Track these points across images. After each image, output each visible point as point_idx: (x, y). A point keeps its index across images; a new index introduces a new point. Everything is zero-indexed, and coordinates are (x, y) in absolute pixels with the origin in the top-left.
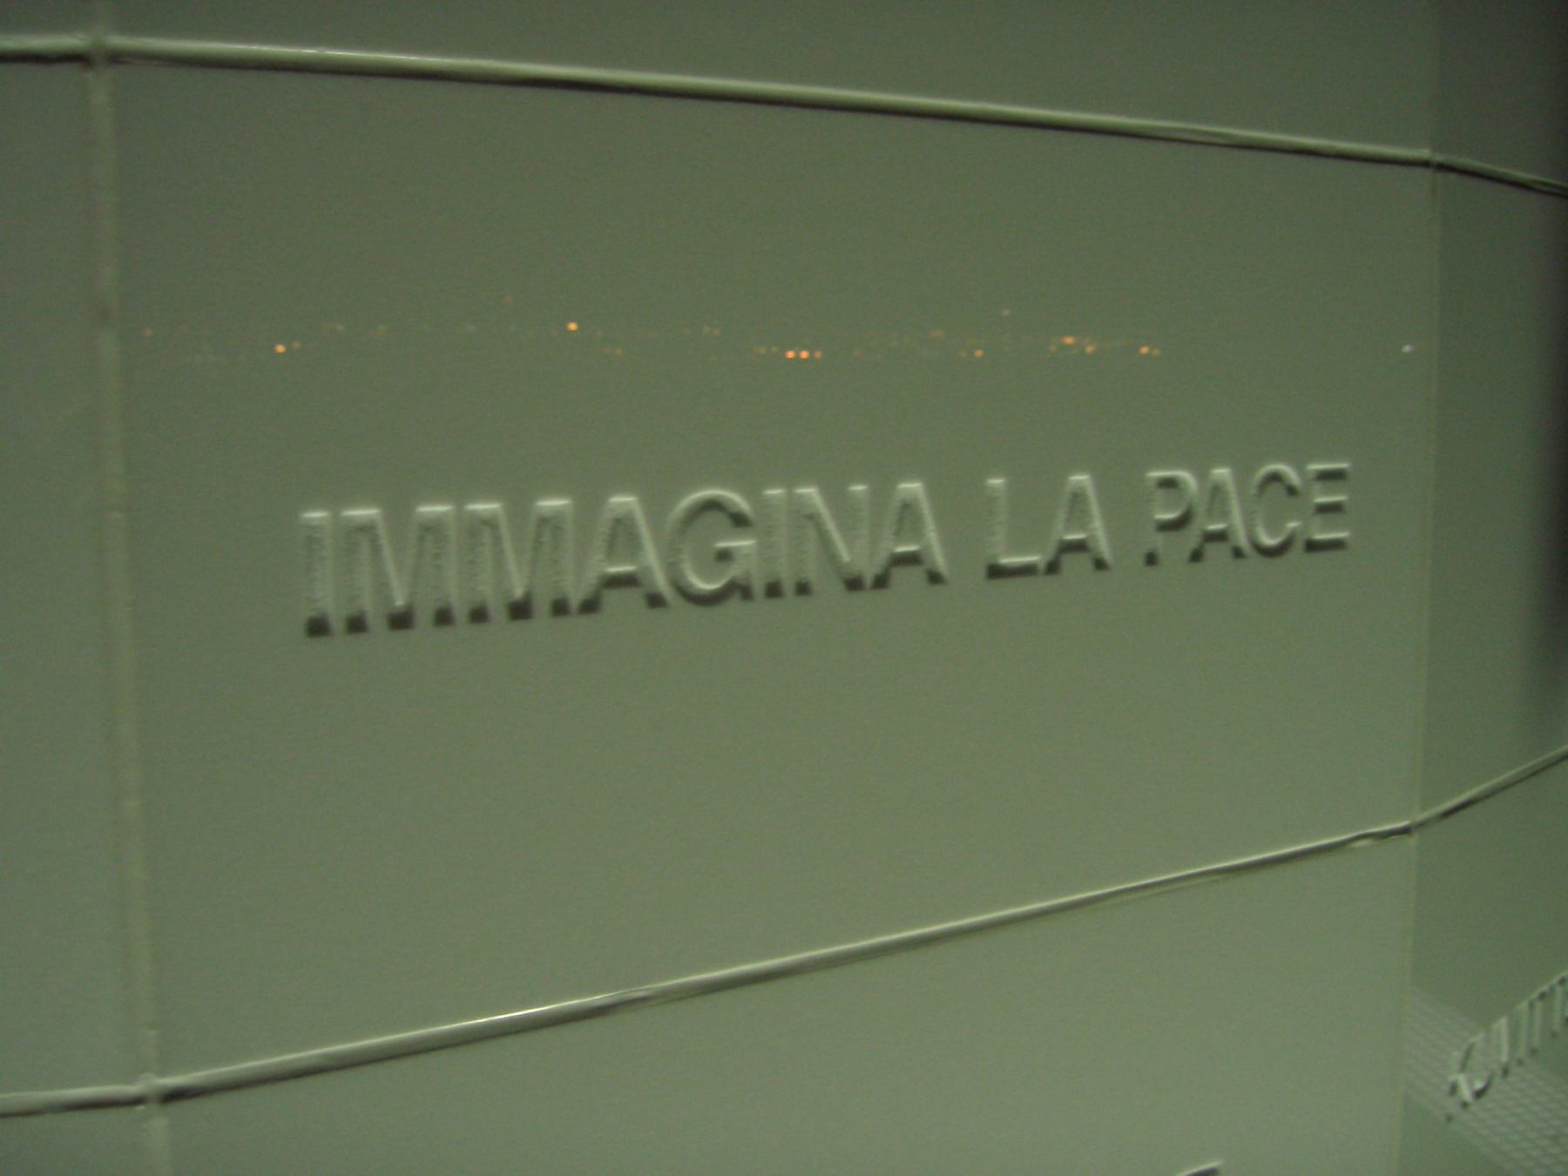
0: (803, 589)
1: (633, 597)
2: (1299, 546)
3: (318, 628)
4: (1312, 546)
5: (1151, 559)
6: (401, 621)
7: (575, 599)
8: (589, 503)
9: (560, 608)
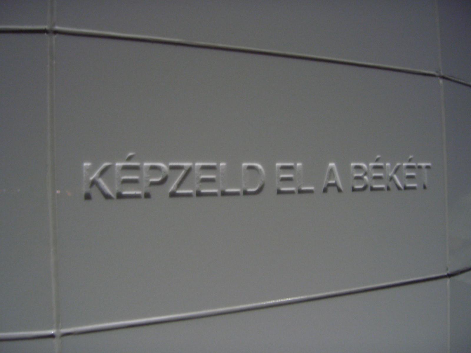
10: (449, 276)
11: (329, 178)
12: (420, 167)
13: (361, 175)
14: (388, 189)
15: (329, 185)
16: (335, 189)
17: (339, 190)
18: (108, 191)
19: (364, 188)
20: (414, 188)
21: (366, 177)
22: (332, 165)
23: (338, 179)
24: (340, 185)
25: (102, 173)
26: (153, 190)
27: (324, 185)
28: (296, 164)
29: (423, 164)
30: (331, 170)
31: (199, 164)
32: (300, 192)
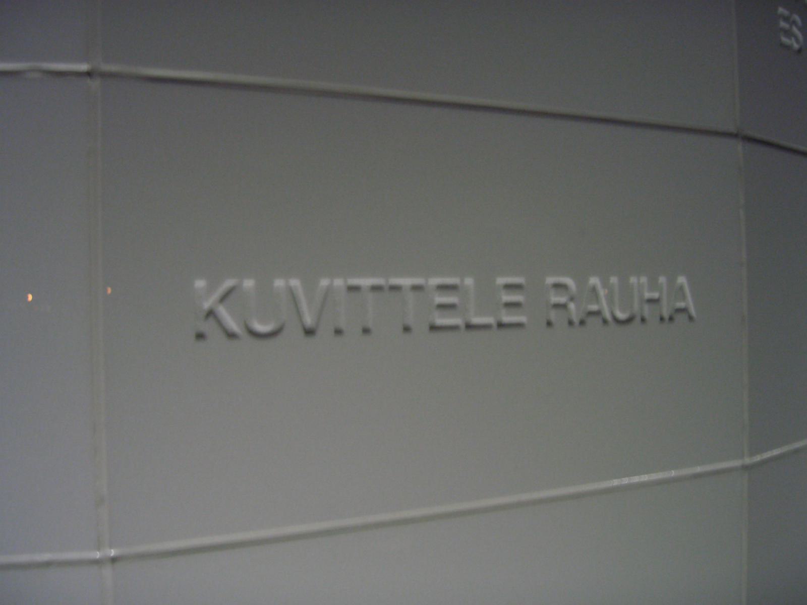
2: (638, 319)
12: (395, 288)
13: (562, 300)
15: (591, 313)
17: (691, 318)
18: (233, 325)
19: (630, 320)
20: (519, 325)
21: (572, 306)
23: (689, 303)
24: (693, 311)
25: (223, 299)
28: (462, 281)
29: (406, 282)
31: (435, 281)
32: (469, 326)
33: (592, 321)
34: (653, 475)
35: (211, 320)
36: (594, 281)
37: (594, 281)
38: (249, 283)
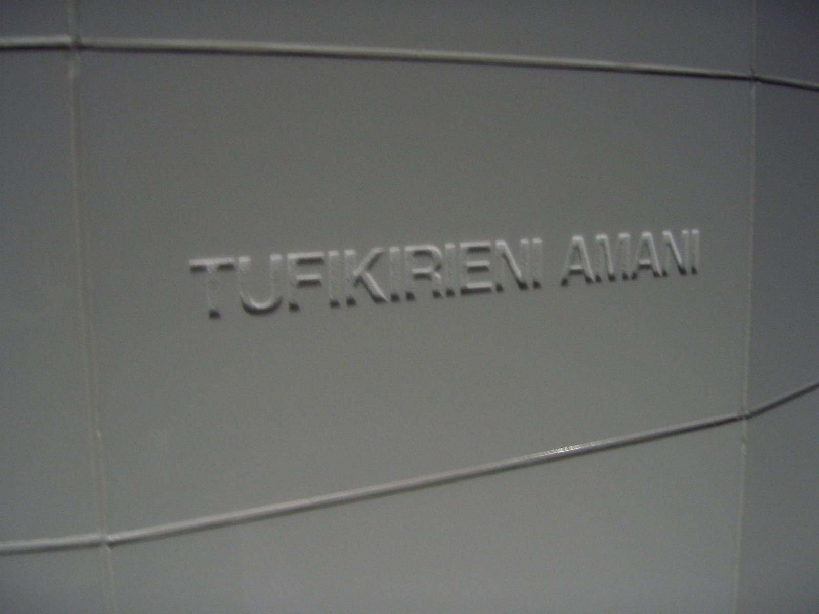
0: (536, 285)
1: (649, 273)
2: (285, 306)
3: (335, 304)
4: (465, 291)
5: (214, 315)
6: (612, 278)
7: (629, 274)
8: (636, 236)
9: (625, 277)
10: (748, 417)
11: (573, 261)
14: (499, 288)
16: (580, 280)
18: (379, 291)
22: (578, 239)
26: (303, 297)
27: (563, 273)
29: (210, 262)
30: (577, 248)
31: (293, 256)
33: (645, 275)
34: (598, 442)
35: (361, 286)
36: (647, 235)
37: (647, 235)
38: (244, 260)
